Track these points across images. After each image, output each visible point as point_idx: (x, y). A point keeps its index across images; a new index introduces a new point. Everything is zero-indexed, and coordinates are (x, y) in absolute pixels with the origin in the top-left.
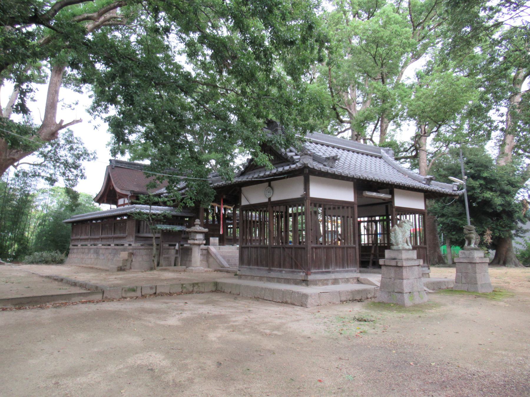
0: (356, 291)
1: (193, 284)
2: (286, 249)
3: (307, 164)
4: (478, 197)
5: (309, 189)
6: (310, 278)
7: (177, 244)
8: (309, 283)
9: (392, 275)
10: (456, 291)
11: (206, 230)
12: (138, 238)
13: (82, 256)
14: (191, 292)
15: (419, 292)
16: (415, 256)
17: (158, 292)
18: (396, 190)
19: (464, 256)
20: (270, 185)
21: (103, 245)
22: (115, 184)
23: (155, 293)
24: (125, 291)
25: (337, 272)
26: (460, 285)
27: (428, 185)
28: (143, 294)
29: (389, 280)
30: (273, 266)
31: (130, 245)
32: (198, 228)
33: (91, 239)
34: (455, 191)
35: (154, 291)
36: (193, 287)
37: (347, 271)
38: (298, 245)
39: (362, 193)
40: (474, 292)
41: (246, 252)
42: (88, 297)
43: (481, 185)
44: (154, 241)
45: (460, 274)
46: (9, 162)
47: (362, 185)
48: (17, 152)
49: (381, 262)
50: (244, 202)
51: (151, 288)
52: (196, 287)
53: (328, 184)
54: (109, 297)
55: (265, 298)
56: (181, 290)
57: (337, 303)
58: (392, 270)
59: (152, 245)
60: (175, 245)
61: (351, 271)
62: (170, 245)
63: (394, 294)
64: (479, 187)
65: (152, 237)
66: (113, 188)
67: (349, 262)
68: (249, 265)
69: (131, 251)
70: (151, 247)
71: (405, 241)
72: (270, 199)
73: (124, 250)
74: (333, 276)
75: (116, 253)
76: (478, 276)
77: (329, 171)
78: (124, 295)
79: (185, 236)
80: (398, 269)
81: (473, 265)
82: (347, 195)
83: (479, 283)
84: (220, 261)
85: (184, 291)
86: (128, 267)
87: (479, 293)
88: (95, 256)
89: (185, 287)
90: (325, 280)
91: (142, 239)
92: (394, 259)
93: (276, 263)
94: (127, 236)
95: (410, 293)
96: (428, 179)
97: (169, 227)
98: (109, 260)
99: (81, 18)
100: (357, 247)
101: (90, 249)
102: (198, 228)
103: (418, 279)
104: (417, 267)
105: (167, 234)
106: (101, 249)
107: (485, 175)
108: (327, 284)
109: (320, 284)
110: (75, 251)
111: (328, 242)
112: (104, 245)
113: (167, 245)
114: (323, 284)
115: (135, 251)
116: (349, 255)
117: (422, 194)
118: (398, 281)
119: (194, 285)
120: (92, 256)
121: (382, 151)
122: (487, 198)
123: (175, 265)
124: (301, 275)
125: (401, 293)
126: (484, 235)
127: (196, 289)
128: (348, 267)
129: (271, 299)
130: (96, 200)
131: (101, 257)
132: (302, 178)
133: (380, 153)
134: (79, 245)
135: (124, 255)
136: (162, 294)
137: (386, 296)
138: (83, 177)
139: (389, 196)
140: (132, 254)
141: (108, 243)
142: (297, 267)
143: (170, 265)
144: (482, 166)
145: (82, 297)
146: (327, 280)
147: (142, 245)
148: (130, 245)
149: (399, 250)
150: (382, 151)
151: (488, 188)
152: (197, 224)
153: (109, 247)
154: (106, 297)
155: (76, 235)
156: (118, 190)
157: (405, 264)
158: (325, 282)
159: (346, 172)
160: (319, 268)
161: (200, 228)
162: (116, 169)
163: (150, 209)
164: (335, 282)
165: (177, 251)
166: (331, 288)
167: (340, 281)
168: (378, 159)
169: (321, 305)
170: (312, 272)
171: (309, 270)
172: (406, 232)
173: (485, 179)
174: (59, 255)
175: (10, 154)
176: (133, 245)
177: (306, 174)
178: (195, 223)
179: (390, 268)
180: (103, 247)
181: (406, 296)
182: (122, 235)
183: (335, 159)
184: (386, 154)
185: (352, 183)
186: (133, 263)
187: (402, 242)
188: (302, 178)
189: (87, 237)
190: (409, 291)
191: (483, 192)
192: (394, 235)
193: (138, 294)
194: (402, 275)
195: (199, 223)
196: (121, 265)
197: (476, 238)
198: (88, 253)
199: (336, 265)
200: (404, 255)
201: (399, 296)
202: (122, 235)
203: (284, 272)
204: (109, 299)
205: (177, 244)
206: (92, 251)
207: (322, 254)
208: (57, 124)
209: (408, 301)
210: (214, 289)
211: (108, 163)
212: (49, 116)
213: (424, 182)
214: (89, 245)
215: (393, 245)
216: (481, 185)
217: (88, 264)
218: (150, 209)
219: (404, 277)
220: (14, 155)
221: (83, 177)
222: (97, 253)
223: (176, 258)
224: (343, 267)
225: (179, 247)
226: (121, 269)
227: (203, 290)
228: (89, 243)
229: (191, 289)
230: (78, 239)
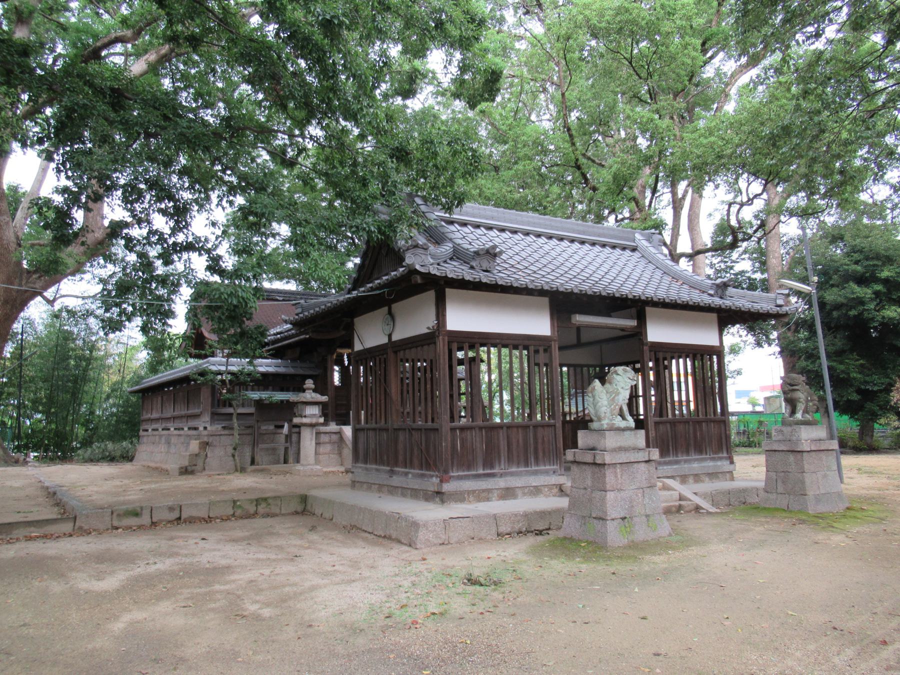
0: (536, 512)
1: (257, 500)
2: (413, 432)
3: (413, 264)
4: (873, 319)
5: (444, 316)
6: (447, 487)
7: (286, 425)
8: (445, 497)
9: (589, 482)
10: (765, 508)
11: (325, 398)
12: (215, 416)
14: (254, 515)
15: (647, 516)
16: (642, 443)
17: (184, 516)
18: (648, 310)
19: (780, 437)
20: (390, 313)
23: (180, 518)
24: (119, 515)
25: (512, 474)
26: (773, 496)
27: (721, 298)
28: (154, 520)
29: (583, 491)
30: (396, 464)
31: (205, 428)
32: (310, 396)
34: (780, 306)
35: (176, 514)
36: (256, 506)
37: (535, 473)
38: (430, 423)
39: (570, 319)
40: (800, 511)
41: (362, 437)
42: (45, 528)
43: (877, 294)
44: (235, 420)
45: (773, 475)
47: (563, 303)
48: (40, 277)
49: (570, 454)
50: (358, 347)
51: (171, 509)
52: (263, 505)
53: (478, 303)
54: (86, 527)
55: (364, 528)
56: (232, 513)
57: (489, 537)
58: (588, 471)
59: (232, 429)
60: (282, 427)
61: (546, 472)
63: (592, 520)
64: (872, 300)
65: (232, 414)
67: (541, 454)
68: (366, 462)
69: (206, 439)
71: (617, 411)
72: (390, 336)
74: (501, 483)
76: (808, 478)
77: (484, 280)
78: (116, 523)
79: (288, 410)
80: (597, 469)
81: (799, 456)
82: (538, 324)
83: (811, 493)
85: (237, 514)
87: (808, 515)
89: (240, 506)
90: (484, 491)
92: (593, 449)
93: (401, 458)
95: (623, 519)
96: (718, 286)
97: (264, 395)
99: (106, 40)
100: (559, 425)
101: (161, 436)
102: (310, 396)
103: (647, 491)
104: (643, 464)
107: (885, 274)
108: (488, 499)
109: (471, 498)
110: (145, 440)
111: (570, 413)
113: (272, 427)
114: (479, 499)
115: (211, 440)
116: (540, 441)
117: (714, 316)
118: (597, 494)
119: (258, 502)
120: (163, 448)
121: (638, 236)
122: (890, 319)
123: (286, 462)
124: (432, 483)
125: (603, 519)
126: (892, 391)
127: (262, 509)
128: (537, 464)
129: (370, 530)
131: (173, 450)
132: (431, 295)
133: (634, 241)
136: (191, 520)
137: (578, 525)
139: (633, 323)
140: (207, 444)
142: (428, 468)
143: (278, 462)
144: (878, 257)
145: (32, 529)
146: (489, 491)
147: (224, 428)
149: (601, 431)
150: (638, 236)
151: (894, 299)
152: (309, 389)
153: (181, 432)
154: (81, 528)
157: (608, 459)
158: (483, 496)
159: (521, 279)
160: (469, 468)
161: (314, 395)
163: (227, 364)
164: (508, 493)
166: (496, 507)
167: (519, 492)
168: (628, 253)
169: (449, 543)
170: (451, 477)
171: (446, 472)
172: (618, 394)
173: (886, 281)
177: (439, 288)
178: (305, 386)
179: (584, 467)
180: (176, 432)
181: (611, 526)
183: (491, 254)
184: (645, 243)
185: (546, 300)
186: (208, 460)
187: (608, 415)
188: (431, 295)
189: (183, 413)
190: (622, 515)
191: (883, 308)
192: (591, 399)
193: (145, 520)
194: (604, 483)
195: (313, 386)
196: (186, 463)
197: (807, 401)
199: (510, 461)
200: (611, 441)
201: (597, 524)
203: (410, 476)
204: (85, 531)
205: (286, 425)
207: (477, 441)
209: (614, 535)
210: (300, 508)
213: (712, 292)
215: (591, 421)
216: (877, 294)
218: (227, 364)
219: (608, 487)
220: (34, 283)
223: (286, 449)
224: (527, 464)
225: (290, 430)
226: (185, 471)
227: (278, 511)
228: (171, 426)
229: (252, 509)
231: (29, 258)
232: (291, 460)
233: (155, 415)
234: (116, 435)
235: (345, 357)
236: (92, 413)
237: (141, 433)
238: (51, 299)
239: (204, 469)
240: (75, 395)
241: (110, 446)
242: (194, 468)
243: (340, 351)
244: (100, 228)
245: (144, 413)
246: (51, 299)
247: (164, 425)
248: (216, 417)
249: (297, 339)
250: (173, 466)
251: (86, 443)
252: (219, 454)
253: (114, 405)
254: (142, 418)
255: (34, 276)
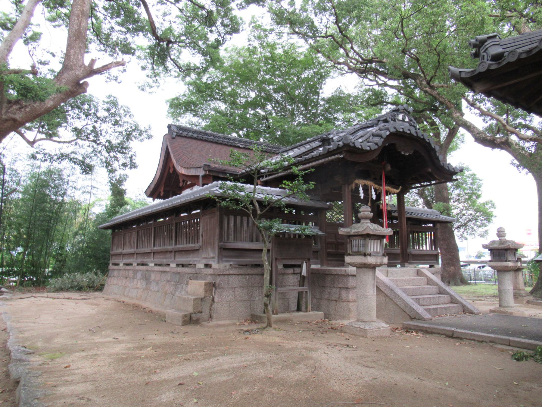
12: (225, 251)
13: (124, 281)
21: (156, 265)
22: (177, 161)
31: (207, 266)
33: (137, 254)
46: (7, 124)
48: (20, 108)
59: (259, 266)
60: (300, 266)
62: (286, 266)
65: (261, 250)
66: (175, 170)
69: (210, 279)
70: (258, 270)
73: (196, 276)
75: (179, 281)
84: (406, 304)
86: (205, 315)
88: (144, 283)
91: (231, 253)
94: (201, 247)
98: (166, 293)
101: (135, 272)
105: (282, 241)
106: (154, 271)
110: (116, 273)
112: (160, 265)
115: (218, 280)
120: (140, 284)
123: (299, 309)
130: (149, 193)
131: (154, 287)
134: (121, 265)
135: (197, 287)
138: (133, 166)
140: (214, 285)
141: (165, 261)
143: (287, 310)
148: (207, 266)
152: (366, 218)
153: (167, 269)
155: (118, 247)
156: (181, 170)
162: (179, 139)
165: (303, 279)
174: (98, 279)
175: (7, 112)
176: (215, 265)
180: (157, 268)
182: (190, 246)
186: (215, 306)
189: (132, 251)
196: (190, 310)
198: (134, 278)
202: (190, 246)
206: (139, 275)
208: (85, 66)
211: (166, 131)
212: (73, 52)
214: (135, 264)
217: (133, 298)
220: (15, 114)
221: (133, 166)
222: (147, 279)
223: (300, 294)
226: (190, 320)
228: (134, 261)
230: (120, 255)
231: (36, 259)
232: (303, 308)
233: (127, 250)
234: (82, 267)
235: (361, 188)
236: (62, 248)
237: (111, 266)
238: (31, 140)
239: (211, 317)
240: (48, 232)
241: (78, 276)
242: (199, 315)
243: (357, 181)
244: (81, 67)
245: (115, 248)
246: (31, 140)
247: (140, 260)
248: (224, 253)
249: (327, 159)
250: (174, 313)
251: (57, 273)
252: (232, 298)
253: (82, 241)
254: (112, 252)
255: (15, 107)
